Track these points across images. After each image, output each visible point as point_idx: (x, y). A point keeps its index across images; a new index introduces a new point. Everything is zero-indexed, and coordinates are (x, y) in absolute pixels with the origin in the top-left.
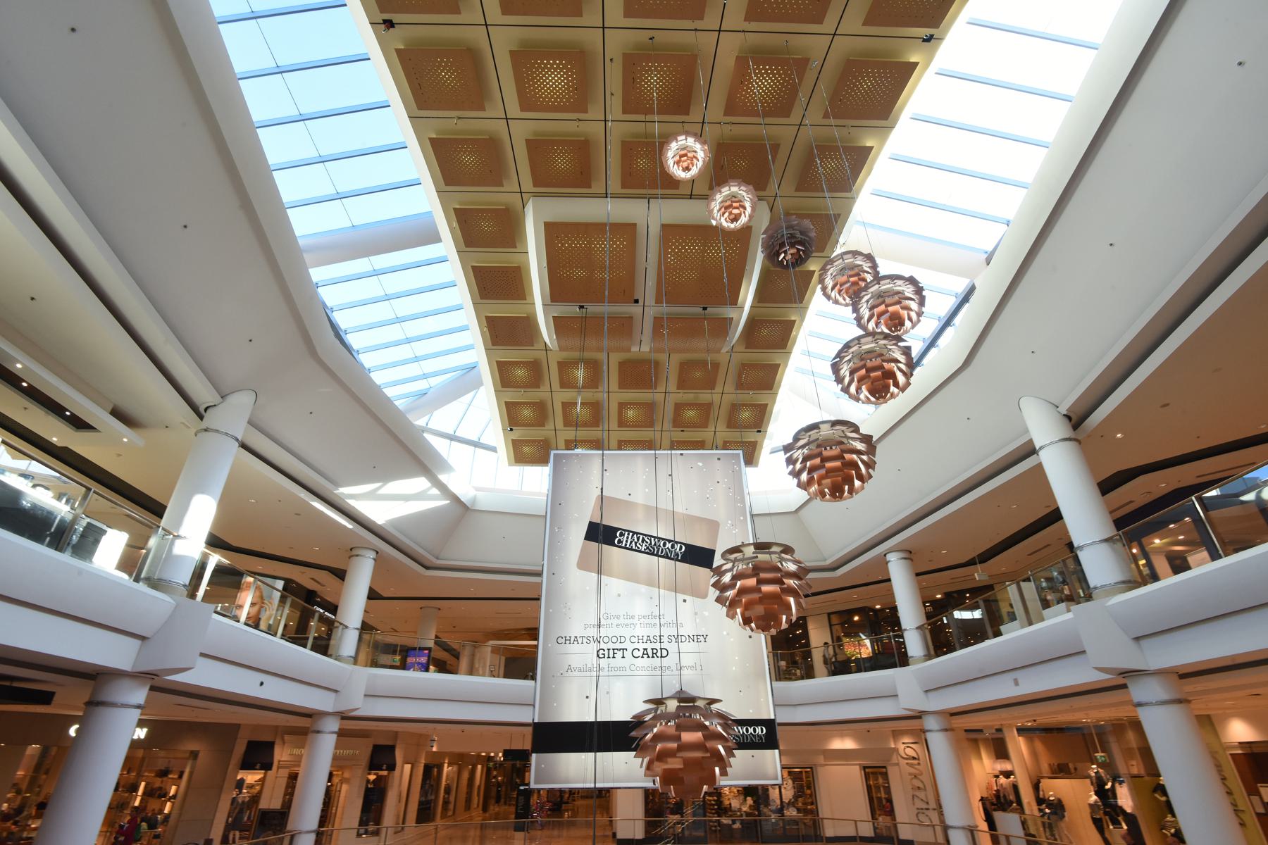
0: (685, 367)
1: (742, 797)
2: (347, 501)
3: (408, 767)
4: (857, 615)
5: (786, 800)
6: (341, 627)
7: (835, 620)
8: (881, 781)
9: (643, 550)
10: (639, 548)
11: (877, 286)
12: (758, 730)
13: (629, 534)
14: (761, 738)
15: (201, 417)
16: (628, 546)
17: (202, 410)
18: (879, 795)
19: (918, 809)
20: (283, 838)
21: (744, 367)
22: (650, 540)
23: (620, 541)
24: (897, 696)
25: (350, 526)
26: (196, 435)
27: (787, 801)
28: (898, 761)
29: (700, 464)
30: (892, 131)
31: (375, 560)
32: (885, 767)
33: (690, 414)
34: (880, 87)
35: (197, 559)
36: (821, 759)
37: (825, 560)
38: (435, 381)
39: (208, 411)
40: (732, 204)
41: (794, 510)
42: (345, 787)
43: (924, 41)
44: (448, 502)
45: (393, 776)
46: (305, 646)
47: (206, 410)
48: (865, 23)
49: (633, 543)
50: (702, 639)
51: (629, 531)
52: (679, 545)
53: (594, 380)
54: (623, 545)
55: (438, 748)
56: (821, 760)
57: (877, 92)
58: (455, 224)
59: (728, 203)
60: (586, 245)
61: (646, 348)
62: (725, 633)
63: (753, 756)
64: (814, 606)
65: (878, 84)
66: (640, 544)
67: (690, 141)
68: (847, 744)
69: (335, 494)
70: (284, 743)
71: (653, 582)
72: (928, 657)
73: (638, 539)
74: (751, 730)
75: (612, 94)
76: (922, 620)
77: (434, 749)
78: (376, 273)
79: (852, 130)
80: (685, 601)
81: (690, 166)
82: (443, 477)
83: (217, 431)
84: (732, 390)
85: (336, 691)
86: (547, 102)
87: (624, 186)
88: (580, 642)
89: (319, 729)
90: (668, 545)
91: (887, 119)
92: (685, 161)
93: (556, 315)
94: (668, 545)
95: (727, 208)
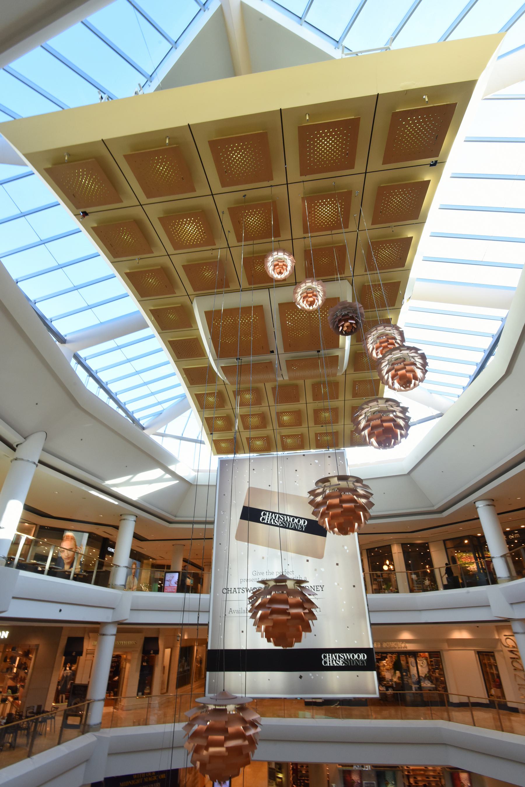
0: (316, 387)
1: (393, 671)
2: (111, 488)
3: (168, 651)
4: (467, 539)
5: (422, 674)
6: (115, 566)
7: (449, 544)
8: (492, 661)
9: (279, 525)
10: (276, 523)
11: (390, 356)
12: (361, 656)
13: (269, 514)
14: (363, 662)
15: (14, 450)
16: (269, 522)
17: (15, 446)
18: (492, 671)
19: (519, 685)
20: (84, 705)
21: (355, 383)
22: (284, 518)
23: (263, 519)
24: (489, 606)
25: (116, 503)
26: (11, 462)
27: (423, 676)
28: (502, 648)
29: (317, 461)
30: (425, 224)
31: (135, 521)
32: (493, 652)
33: (326, 415)
34: (406, 200)
35: (12, 540)
36: (445, 646)
37: (433, 506)
38: (166, 405)
39: (19, 446)
40: (309, 294)
41: (406, 473)
42: (128, 665)
43: (431, 165)
44: (178, 481)
45: (158, 658)
46: (90, 583)
47: (17, 446)
48: (384, 163)
49: (272, 520)
50: (320, 588)
51: (269, 512)
52: (303, 520)
53: (258, 400)
54: (266, 522)
55: (188, 636)
56: (445, 646)
57: (405, 203)
58: (153, 318)
59: (305, 294)
60: (232, 322)
61: (286, 378)
62: (336, 584)
63: (358, 676)
64: (433, 535)
65: (405, 198)
66: (276, 521)
67: (281, 255)
68: (463, 635)
69: (104, 486)
70: (89, 638)
71: (282, 547)
72: (512, 578)
73: (275, 517)
74: (356, 656)
75: (229, 231)
76: (506, 551)
77: (186, 637)
78: (119, 347)
79: (394, 229)
80: (308, 561)
81: (282, 271)
82: (172, 467)
83: (22, 459)
84: (351, 398)
85: (113, 609)
86: (249, 212)
87: (250, 283)
88: (238, 592)
89: (104, 633)
90: (296, 521)
91: (418, 219)
92: (277, 269)
93: (223, 365)
94: (296, 521)
95: (304, 298)
